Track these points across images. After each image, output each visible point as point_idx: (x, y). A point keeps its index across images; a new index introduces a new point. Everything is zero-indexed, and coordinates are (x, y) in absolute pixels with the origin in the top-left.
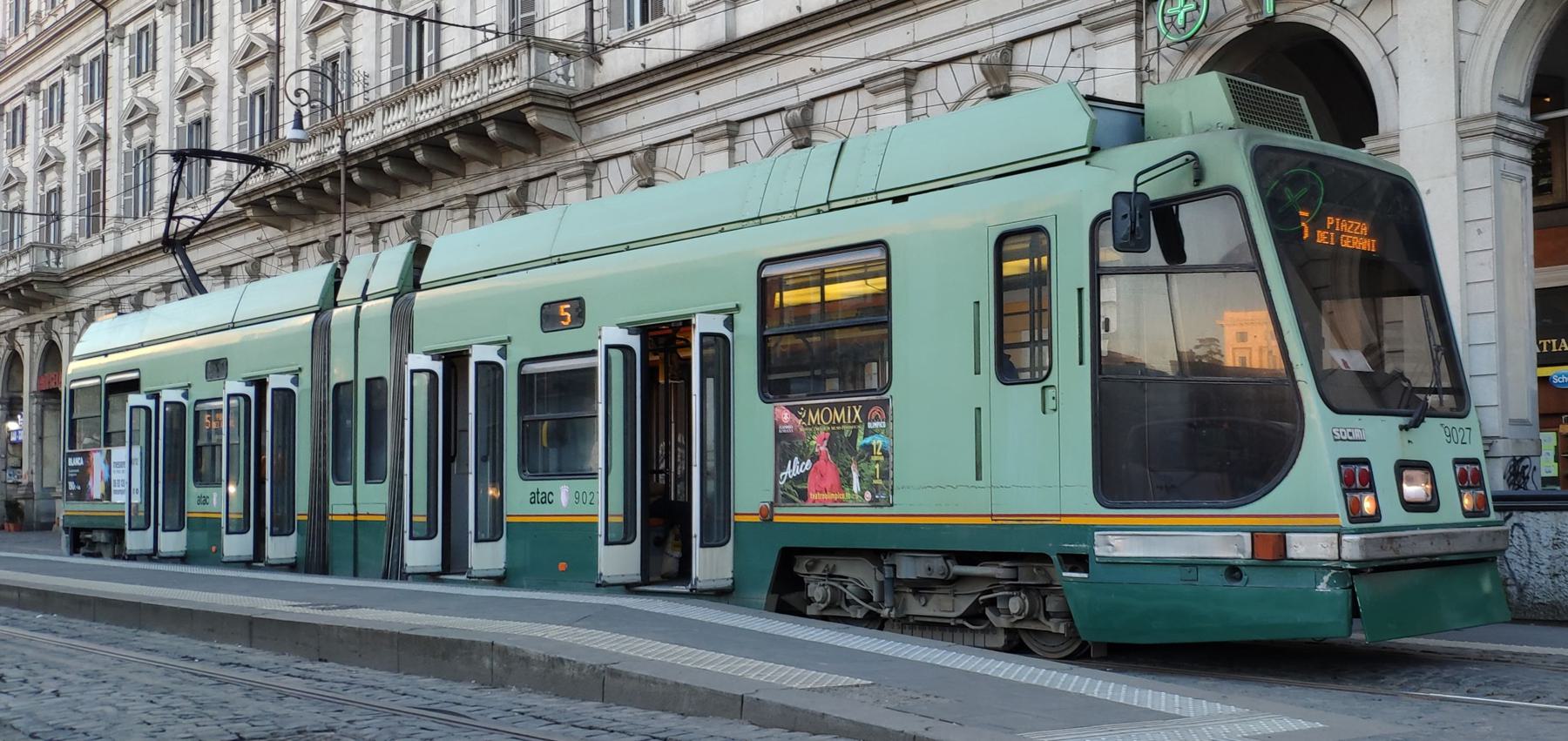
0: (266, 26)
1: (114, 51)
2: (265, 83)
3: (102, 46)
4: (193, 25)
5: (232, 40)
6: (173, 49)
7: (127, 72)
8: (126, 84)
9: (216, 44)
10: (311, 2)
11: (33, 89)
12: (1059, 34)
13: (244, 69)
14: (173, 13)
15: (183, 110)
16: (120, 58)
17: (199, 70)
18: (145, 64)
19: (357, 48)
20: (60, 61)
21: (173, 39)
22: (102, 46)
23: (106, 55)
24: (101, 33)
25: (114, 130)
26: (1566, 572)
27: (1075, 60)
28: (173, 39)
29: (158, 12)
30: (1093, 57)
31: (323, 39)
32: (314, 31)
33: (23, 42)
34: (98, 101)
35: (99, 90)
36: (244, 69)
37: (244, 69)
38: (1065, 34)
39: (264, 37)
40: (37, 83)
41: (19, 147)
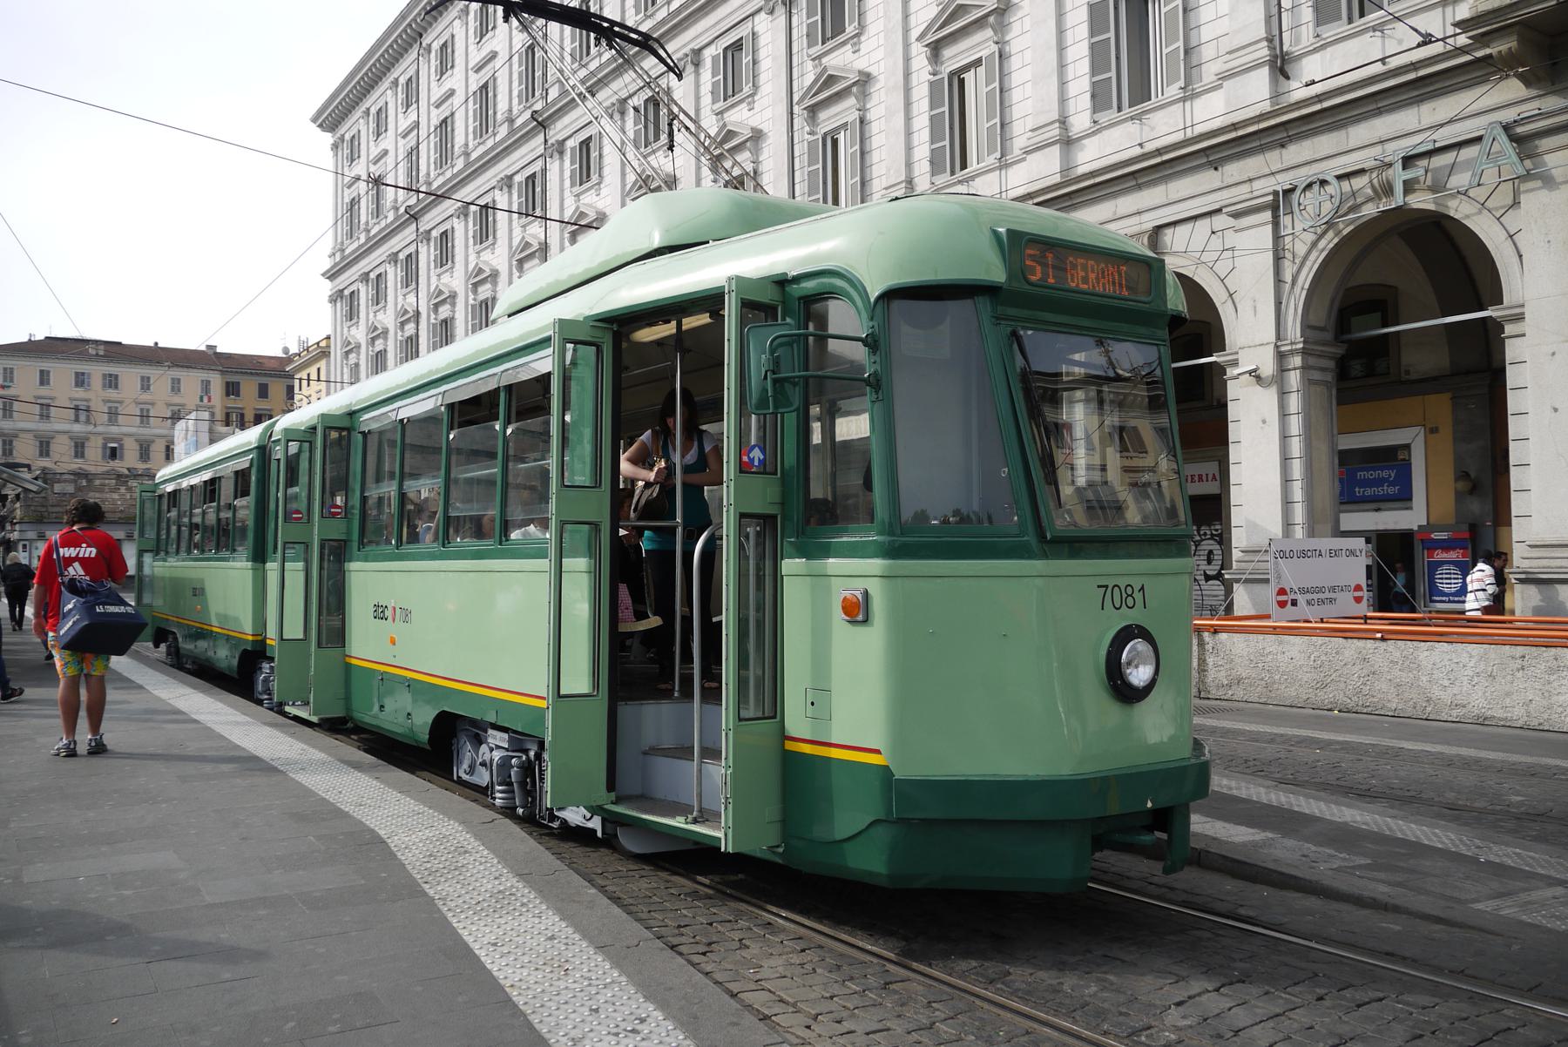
0: (411, 298)
1: (423, 249)
2: (413, 332)
3: (540, 163)
4: (725, 78)
5: (510, 239)
6: (467, 247)
7: (471, 241)
8: (567, 193)
9: (499, 242)
10: (926, 4)
11: (365, 277)
12: (1200, 223)
13: (521, 262)
14: (561, 159)
15: (475, 292)
16: (427, 254)
17: (485, 262)
18: (445, 257)
19: (763, 168)
20: (384, 258)
21: (467, 239)
22: (540, 163)
23: (544, 171)
24: (541, 150)
25: (423, 309)
26: (17, 584)
27: (1216, 243)
28: (467, 239)
29: (497, 192)
30: (1231, 239)
31: (480, 289)
32: (937, 41)
33: (356, 245)
34: (414, 285)
35: (411, 278)
36: (475, 285)
37: (475, 285)
38: (1206, 222)
39: (534, 236)
40: (510, 177)
41: (594, 178)
